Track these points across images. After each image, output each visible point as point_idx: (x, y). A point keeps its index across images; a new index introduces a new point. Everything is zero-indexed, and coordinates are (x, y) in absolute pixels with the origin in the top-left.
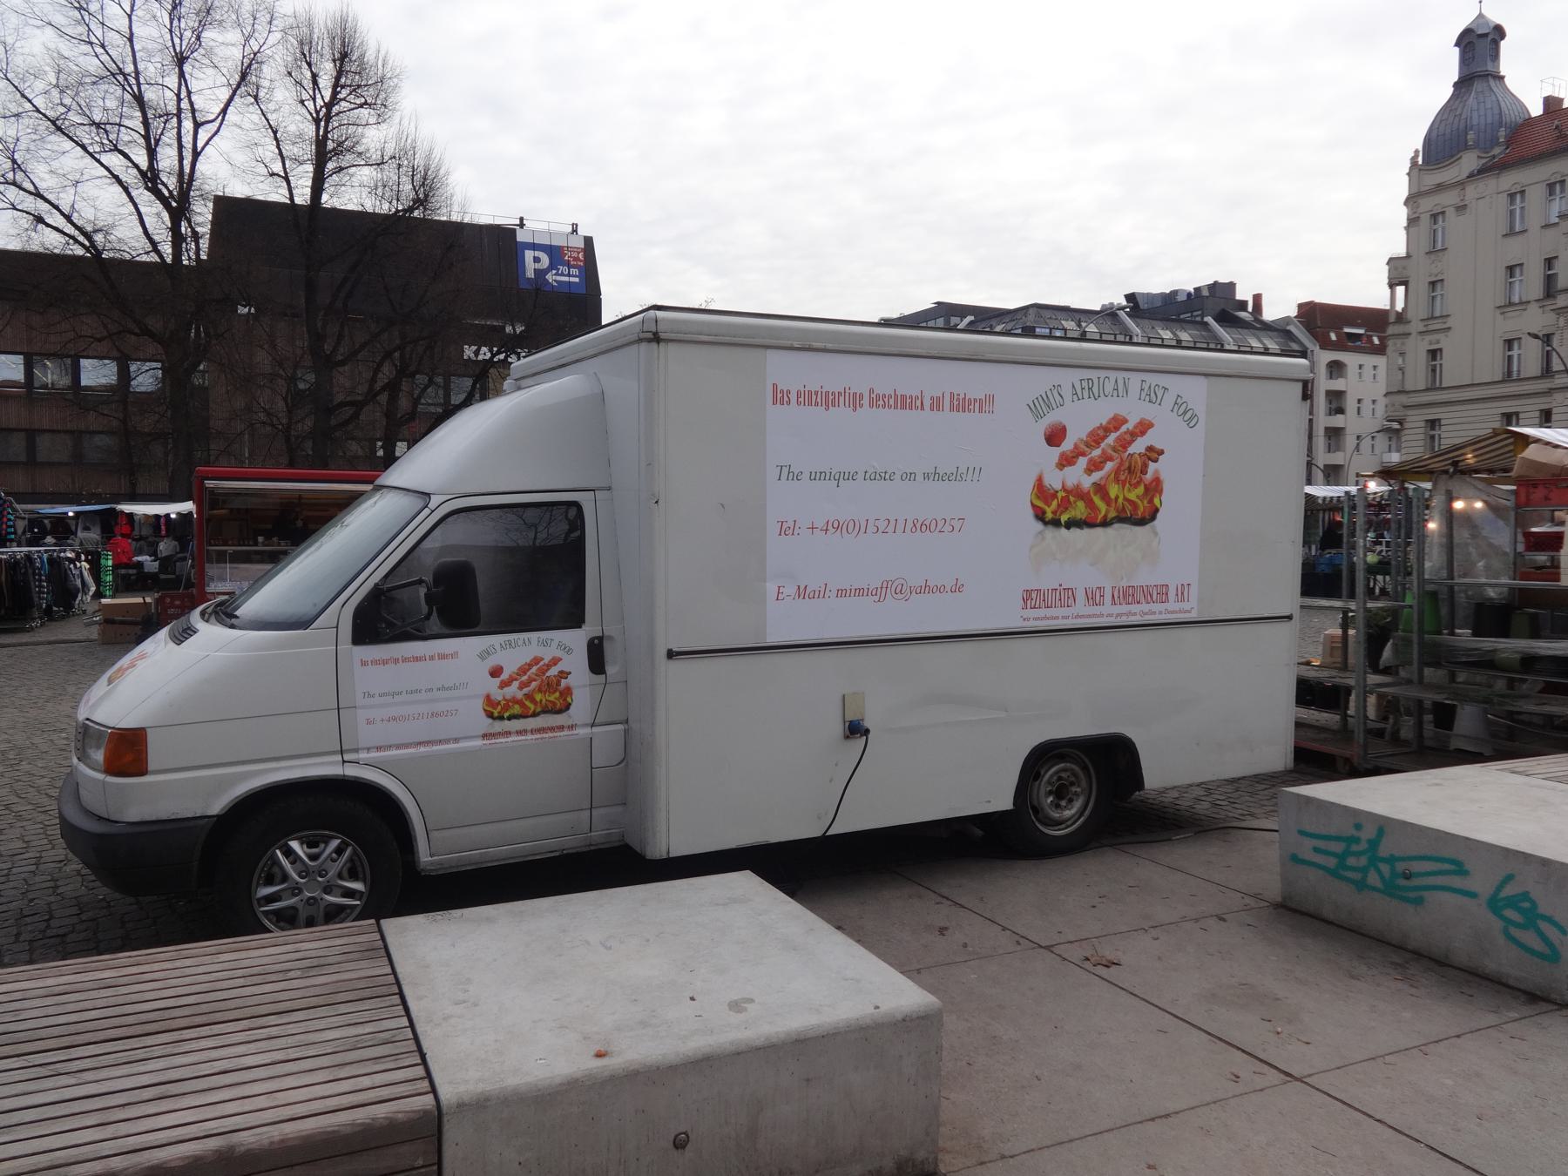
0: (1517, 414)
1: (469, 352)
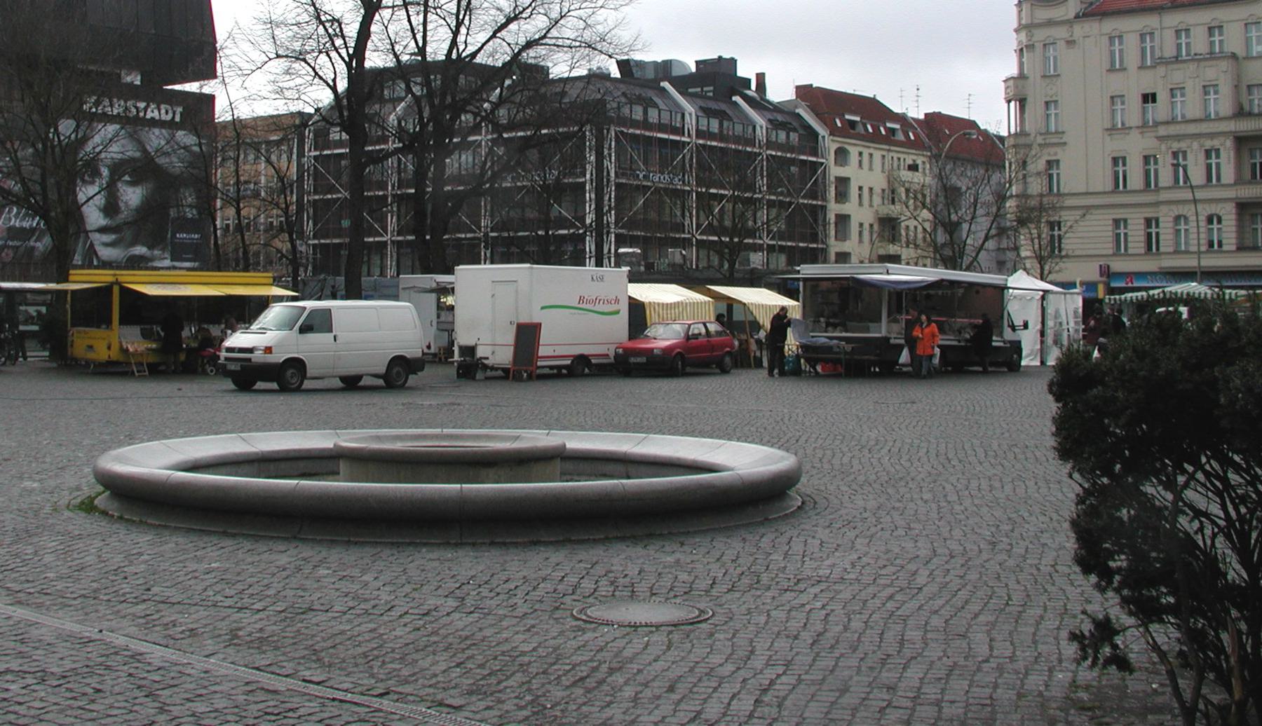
0: (1125, 221)
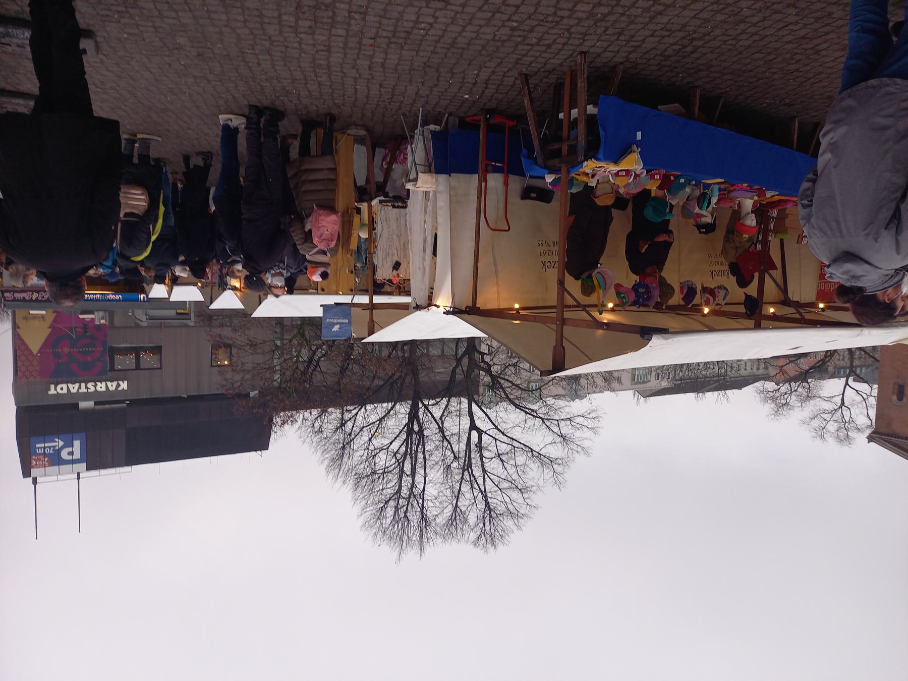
1: (124, 385)
